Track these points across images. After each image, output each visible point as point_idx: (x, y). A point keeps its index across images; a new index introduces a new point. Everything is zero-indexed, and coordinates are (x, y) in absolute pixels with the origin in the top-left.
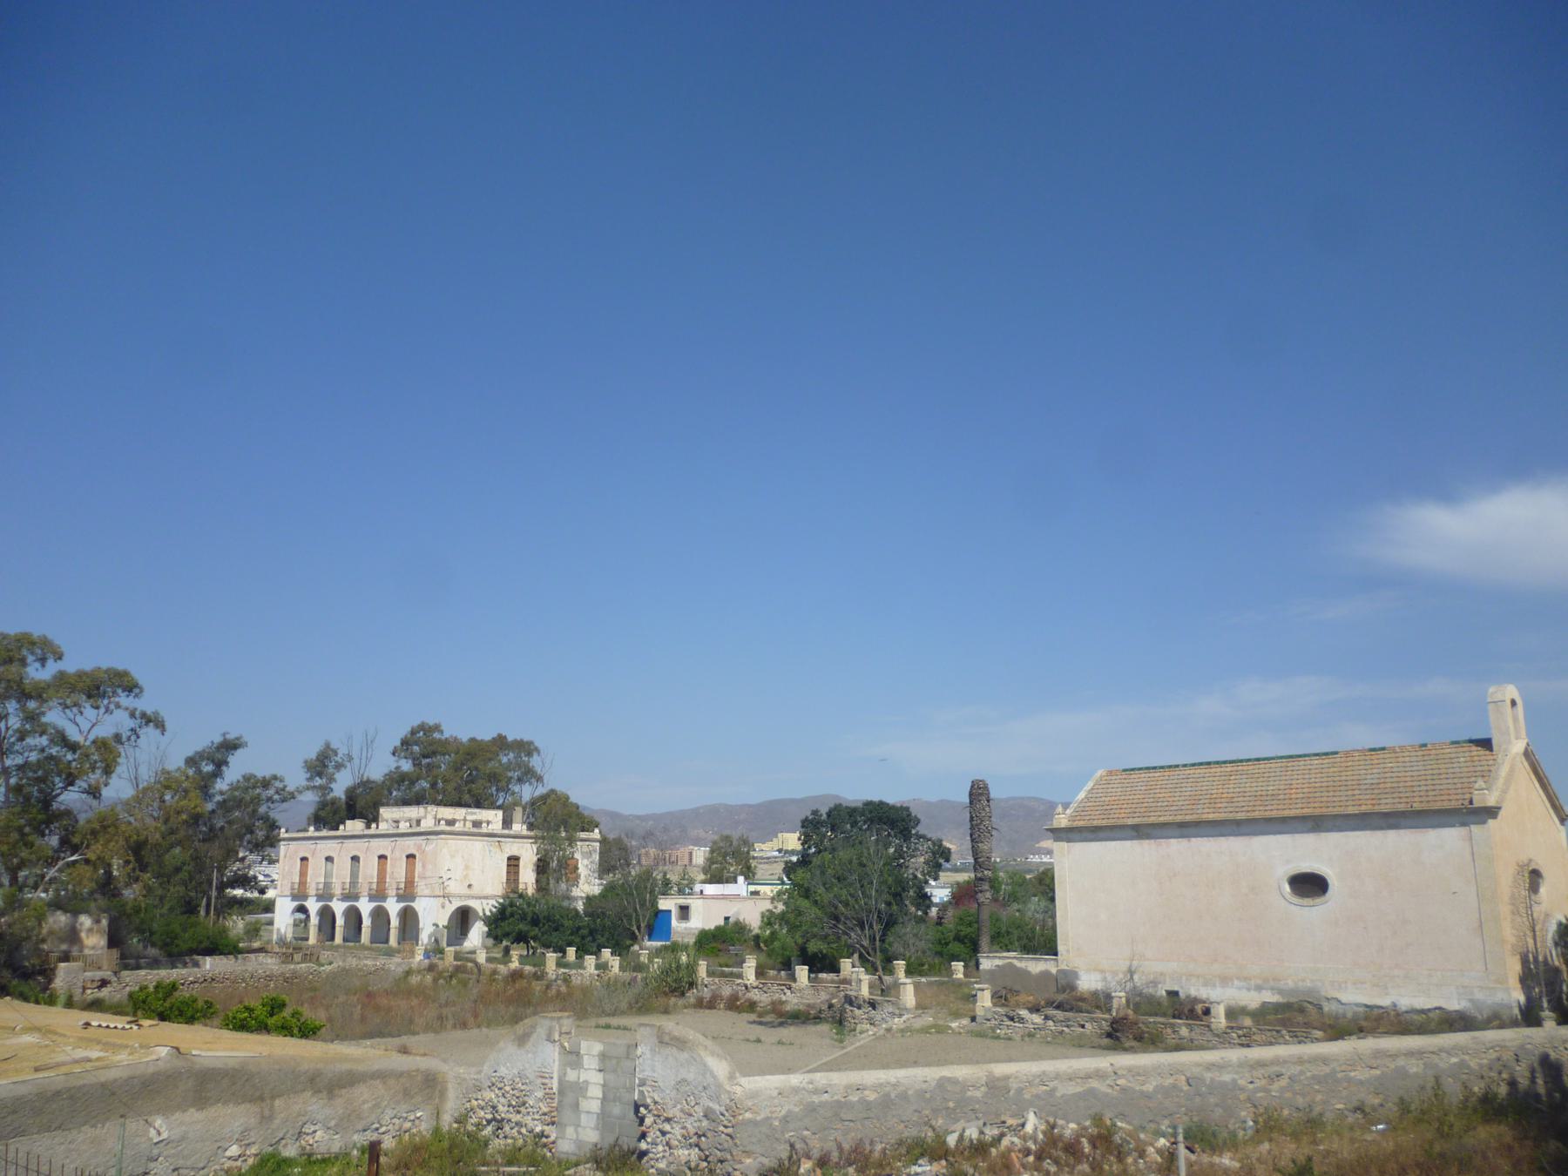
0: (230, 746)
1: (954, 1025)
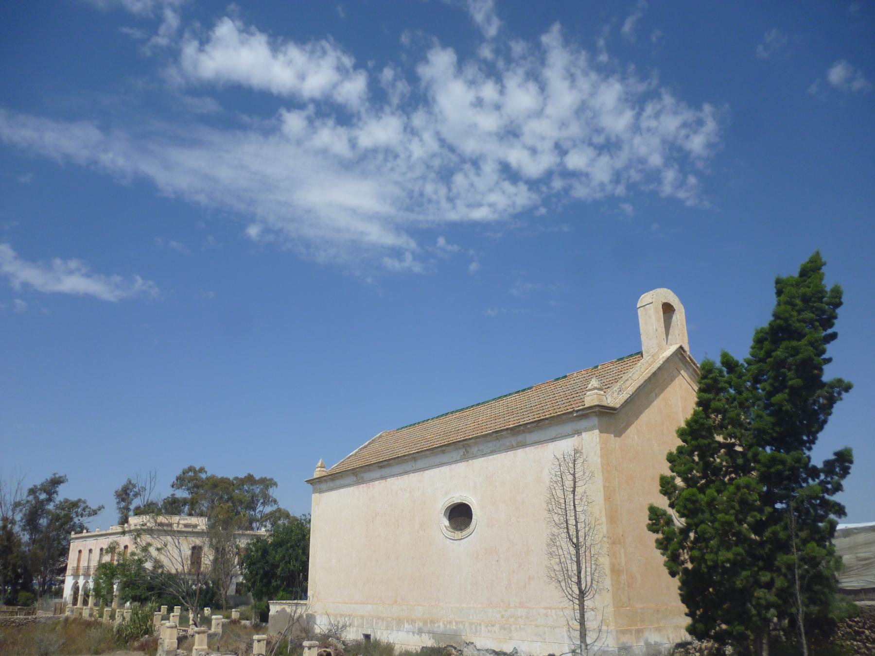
0: (56, 482)
1: (724, 626)
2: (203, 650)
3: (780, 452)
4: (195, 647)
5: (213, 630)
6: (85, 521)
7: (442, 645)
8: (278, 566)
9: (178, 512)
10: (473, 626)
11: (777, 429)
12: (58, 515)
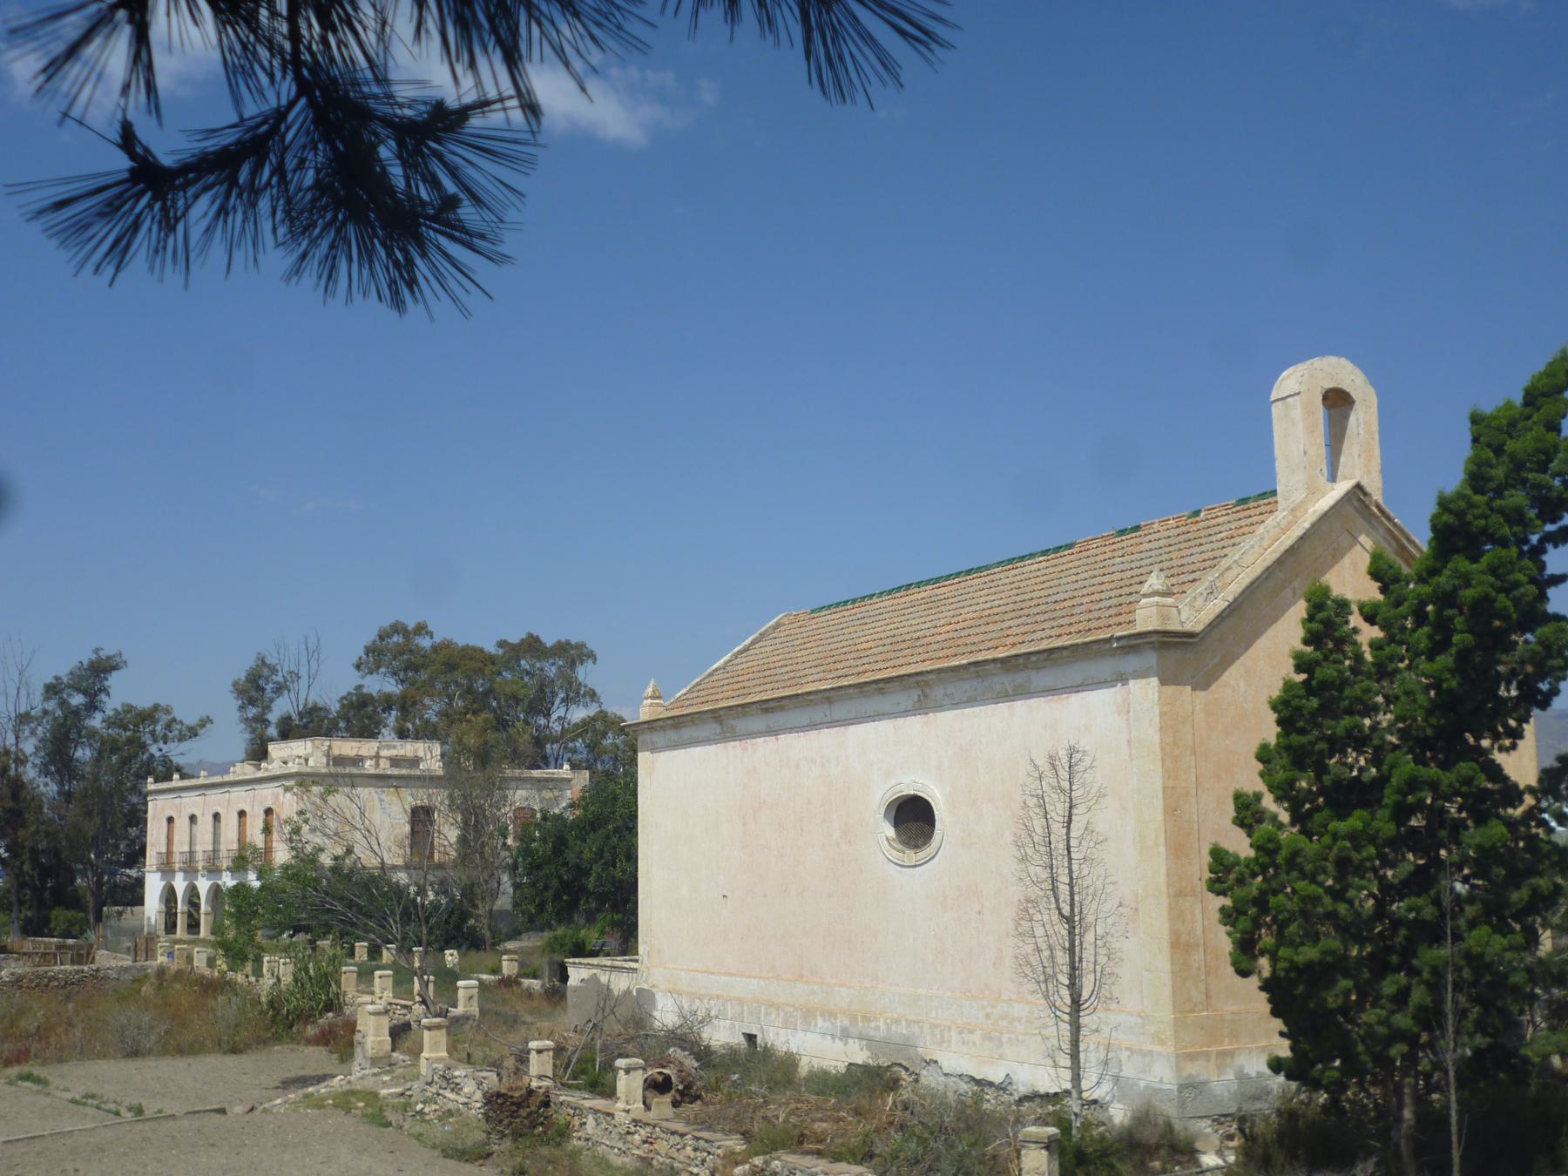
0: (100, 669)
2: (440, 1060)
3: (1425, 764)
4: (425, 1054)
5: (460, 1010)
6: (178, 752)
7: (884, 1062)
8: (587, 873)
9: (367, 731)
10: (937, 1031)
11: (1433, 721)
12: (114, 741)
